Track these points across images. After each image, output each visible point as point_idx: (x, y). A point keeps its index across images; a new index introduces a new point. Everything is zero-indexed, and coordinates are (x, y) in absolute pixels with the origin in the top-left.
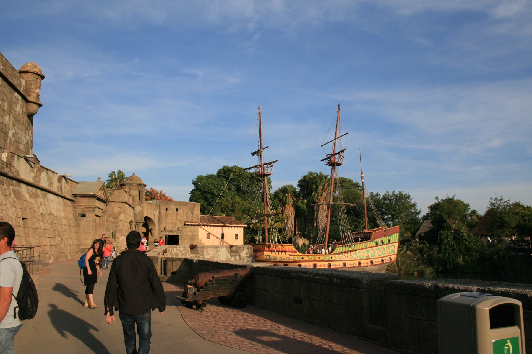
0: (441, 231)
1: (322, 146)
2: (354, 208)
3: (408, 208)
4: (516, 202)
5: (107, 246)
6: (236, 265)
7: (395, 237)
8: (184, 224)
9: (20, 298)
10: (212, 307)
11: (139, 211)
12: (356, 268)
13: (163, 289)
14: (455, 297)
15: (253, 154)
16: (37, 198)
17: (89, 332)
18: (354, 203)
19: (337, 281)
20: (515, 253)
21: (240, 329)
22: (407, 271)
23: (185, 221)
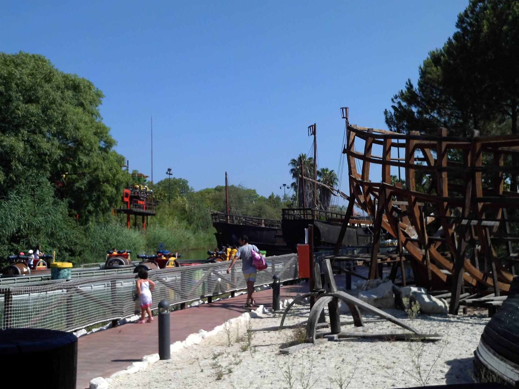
0: (476, 382)
2: (117, 323)
3: (446, 327)
5: (272, 307)
7: (371, 163)
8: (182, 309)
10: (358, 333)
11: (282, 217)
13: (148, 354)
16: (284, 342)
20: (401, 258)
23: (216, 353)
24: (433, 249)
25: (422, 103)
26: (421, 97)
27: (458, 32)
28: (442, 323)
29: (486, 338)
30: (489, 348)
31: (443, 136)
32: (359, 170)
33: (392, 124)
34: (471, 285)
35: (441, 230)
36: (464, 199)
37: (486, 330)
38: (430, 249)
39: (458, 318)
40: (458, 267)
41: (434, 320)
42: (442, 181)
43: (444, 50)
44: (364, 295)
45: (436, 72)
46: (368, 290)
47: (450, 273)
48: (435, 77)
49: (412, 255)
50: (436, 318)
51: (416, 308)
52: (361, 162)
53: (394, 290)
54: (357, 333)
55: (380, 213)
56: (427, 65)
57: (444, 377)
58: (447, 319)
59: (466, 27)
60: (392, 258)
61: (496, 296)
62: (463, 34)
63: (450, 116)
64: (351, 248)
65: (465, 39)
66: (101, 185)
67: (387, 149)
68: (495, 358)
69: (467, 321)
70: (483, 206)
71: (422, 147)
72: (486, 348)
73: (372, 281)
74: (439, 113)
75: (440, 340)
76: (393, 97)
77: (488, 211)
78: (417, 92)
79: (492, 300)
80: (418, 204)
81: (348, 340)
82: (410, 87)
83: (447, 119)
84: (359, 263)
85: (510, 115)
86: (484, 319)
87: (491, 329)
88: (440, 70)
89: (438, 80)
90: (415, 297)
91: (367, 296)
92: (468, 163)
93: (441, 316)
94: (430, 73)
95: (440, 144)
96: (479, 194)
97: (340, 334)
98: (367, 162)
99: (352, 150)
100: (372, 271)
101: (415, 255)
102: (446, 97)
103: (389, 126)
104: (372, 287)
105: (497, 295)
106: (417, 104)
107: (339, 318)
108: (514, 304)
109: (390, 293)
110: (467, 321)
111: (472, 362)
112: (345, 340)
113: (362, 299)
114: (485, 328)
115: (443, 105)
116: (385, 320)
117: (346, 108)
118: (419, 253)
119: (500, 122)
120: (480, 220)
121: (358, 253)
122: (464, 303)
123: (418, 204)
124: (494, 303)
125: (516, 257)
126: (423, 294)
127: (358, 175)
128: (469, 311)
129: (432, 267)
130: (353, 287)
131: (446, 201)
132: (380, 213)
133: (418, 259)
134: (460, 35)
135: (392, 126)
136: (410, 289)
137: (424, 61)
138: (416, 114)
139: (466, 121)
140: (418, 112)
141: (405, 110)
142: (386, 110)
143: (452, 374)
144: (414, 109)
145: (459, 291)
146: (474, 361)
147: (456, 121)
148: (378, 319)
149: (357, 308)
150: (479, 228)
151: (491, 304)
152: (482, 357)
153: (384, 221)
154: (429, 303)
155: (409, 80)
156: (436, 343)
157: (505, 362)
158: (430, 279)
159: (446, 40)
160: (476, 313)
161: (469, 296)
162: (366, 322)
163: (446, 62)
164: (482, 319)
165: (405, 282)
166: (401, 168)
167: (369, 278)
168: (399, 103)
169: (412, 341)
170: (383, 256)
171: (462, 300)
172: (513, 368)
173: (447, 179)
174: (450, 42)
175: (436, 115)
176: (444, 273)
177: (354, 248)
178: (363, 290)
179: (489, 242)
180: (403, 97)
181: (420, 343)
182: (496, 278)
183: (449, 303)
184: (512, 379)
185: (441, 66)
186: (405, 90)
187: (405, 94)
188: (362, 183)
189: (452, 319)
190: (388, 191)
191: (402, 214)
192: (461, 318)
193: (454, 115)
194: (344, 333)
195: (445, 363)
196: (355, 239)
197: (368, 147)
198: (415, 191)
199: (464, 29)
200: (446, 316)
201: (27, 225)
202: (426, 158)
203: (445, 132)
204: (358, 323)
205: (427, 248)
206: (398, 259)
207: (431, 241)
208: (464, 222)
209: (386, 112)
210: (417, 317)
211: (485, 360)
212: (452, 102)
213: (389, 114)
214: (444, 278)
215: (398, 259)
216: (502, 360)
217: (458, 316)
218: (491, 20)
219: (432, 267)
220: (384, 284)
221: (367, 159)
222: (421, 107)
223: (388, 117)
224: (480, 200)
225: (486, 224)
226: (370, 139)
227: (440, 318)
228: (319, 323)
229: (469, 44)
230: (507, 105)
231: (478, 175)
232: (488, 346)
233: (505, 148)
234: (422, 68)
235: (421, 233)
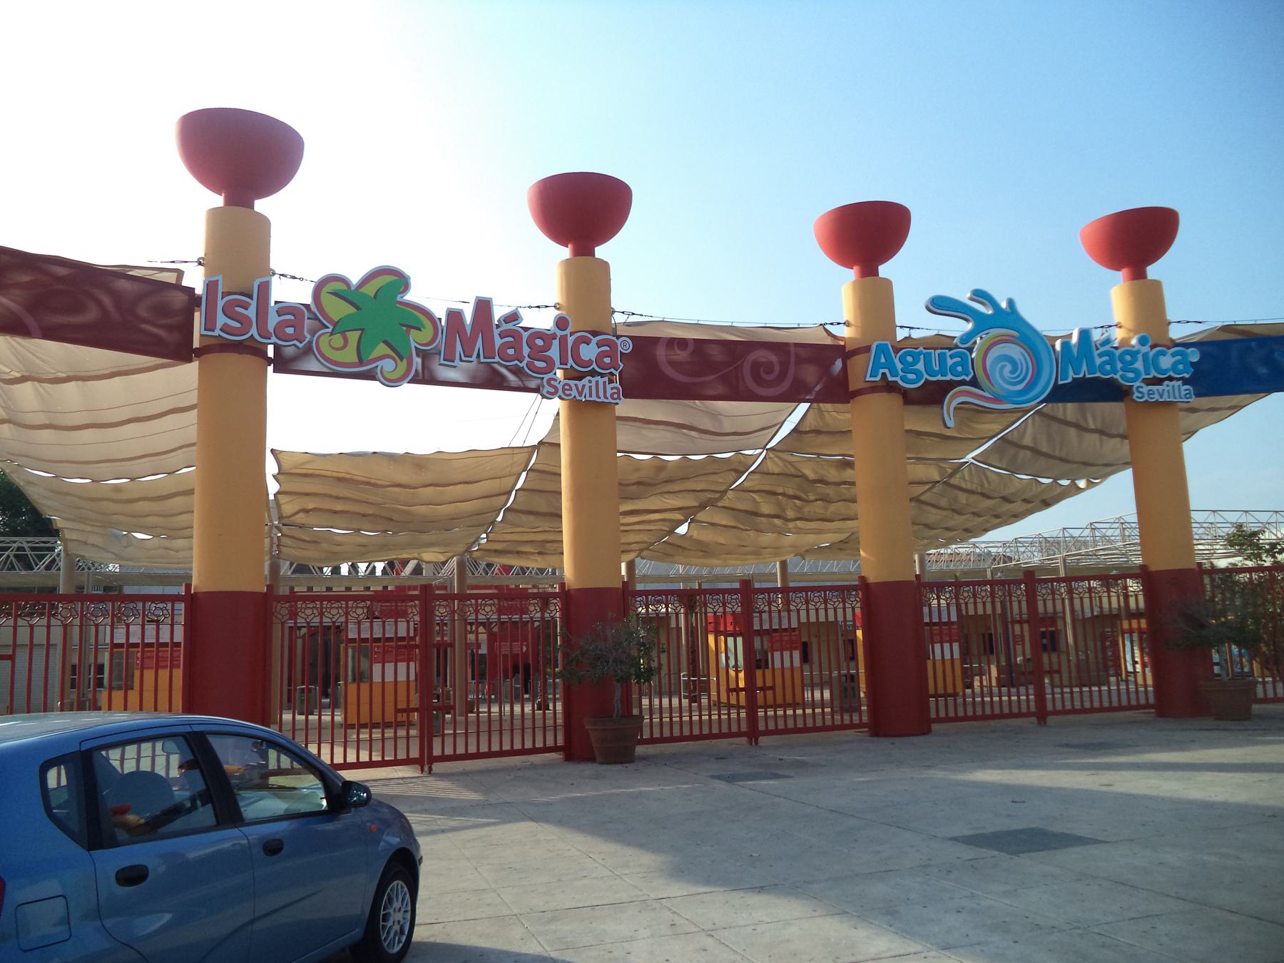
1: (1013, 802)
4: (483, 306)
7: (413, 940)
15: (911, 500)
17: (67, 783)
66: (1135, 332)
77: (955, 627)
87: (331, 944)
92: (927, 686)
114: (161, 776)
130: (1037, 417)
137: (194, 289)
166: (126, 757)
201: (1218, 678)
228: (870, 377)
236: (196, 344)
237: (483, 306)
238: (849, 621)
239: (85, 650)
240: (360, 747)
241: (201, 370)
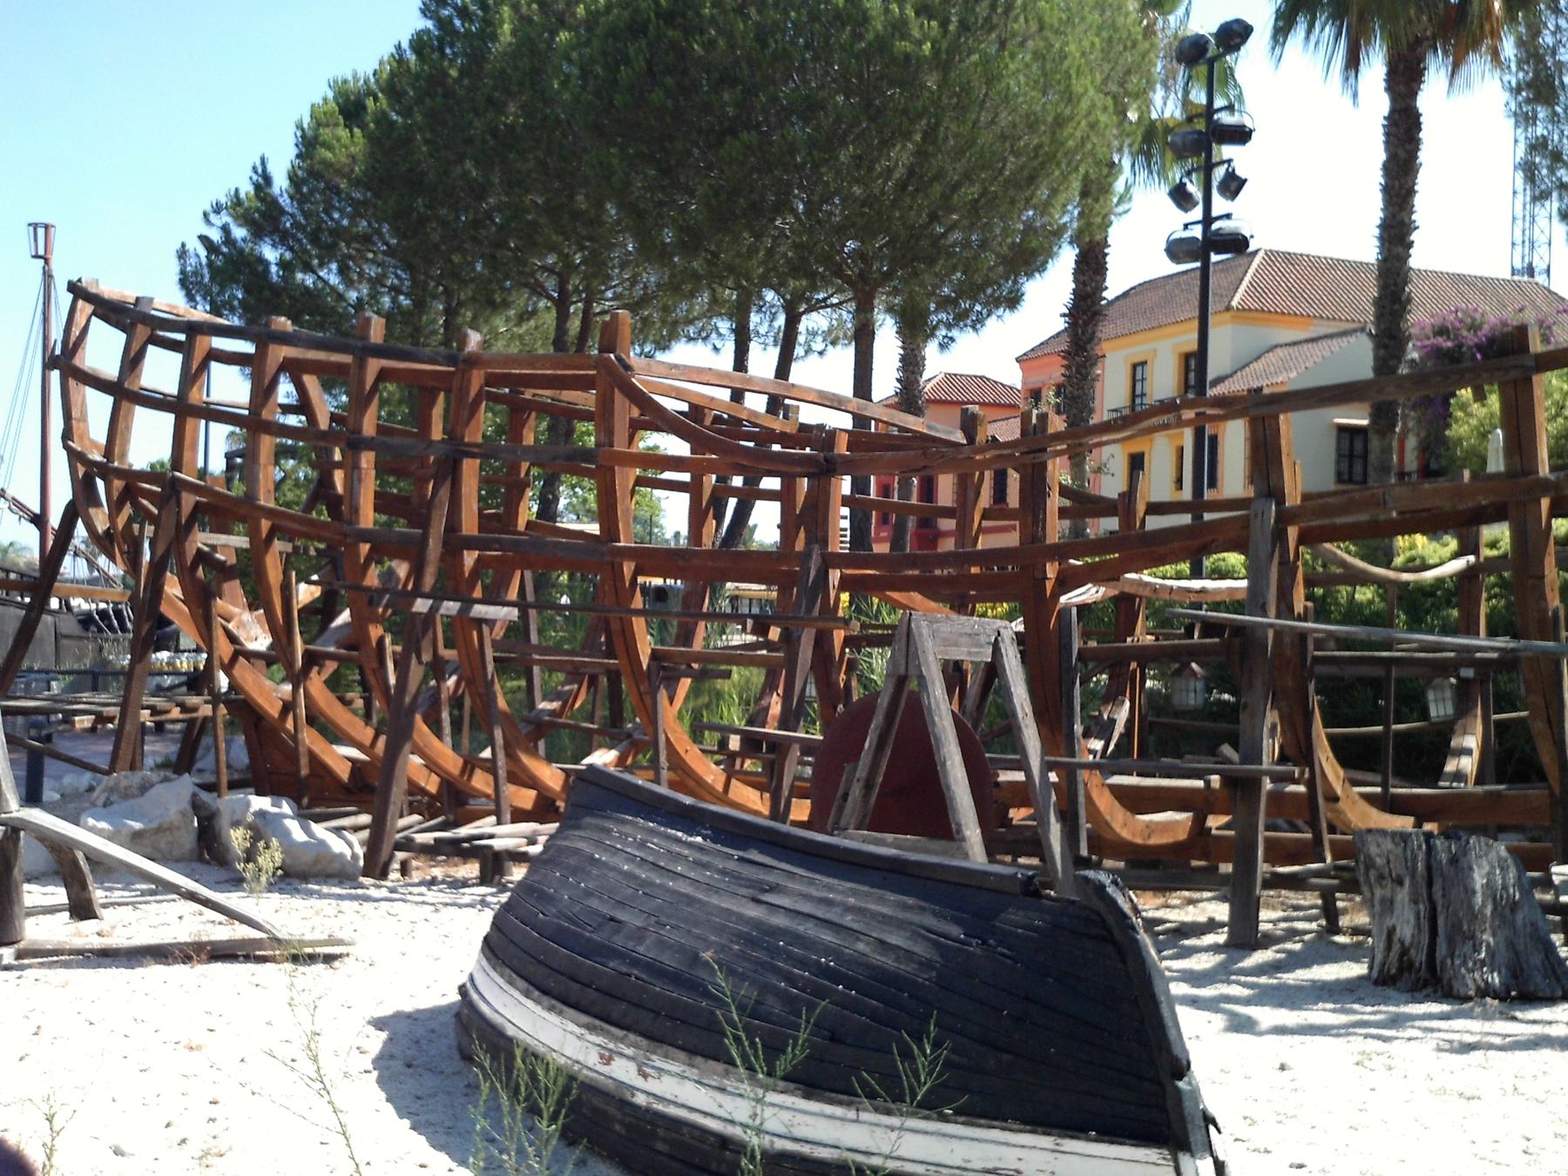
4: (1064, 315)
6: (1411, 192)
9: (1323, 29)
12: (714, 1084)
14: (1196, 765)
18: (819, 1004)
19: (821, 211)
20: (215, 710)
21: (1185, 1063)
22: (1133, 62)
24: (316, 683)
25: (294, 237)
26: (293, 216)
27: (427, 31)
28: (346, 904)
29: (497, 948)
30: (510, 976)
31: (373, 340)
32: (97, 428)
33: (197, 291)
34: (423, 792)
35: (346, 625)
36: (424, 539)
37: (497, 924)
38: (308, 683)
39: (392, 890)
40: (397, 733)
41: (322, 896)
42: (360, 480)
43: (377, 81)
44: (98, 820)
45: (349, 144)
46: (112, 803)
47: (363, 757)
48: (343, 159)
49: (253, 699)
50: (325, 889)
51: (268, 860)
52: (109, 400)
53: (196, 806)
54: (79, 943)
55: (158, 569)
56: (320, 119)
57: (370, 1067)
58: (360, 891)
59: (450, 17)
60: (184, 708)
61: (499, 823)
62: (440, 39)
63: (376, 282)
64: (43, 676)
65: (443, 55)
67: (195, 367)
68: (530, 1003)
69: (420, 899)
70: (479, 560)
71: (294, 369)
72: (502, 976)
73: (126, 777)
74: (343, 271)
75: (348, 955)
76: (209, 209)
78: (285, 201)
79: (491, 836)
80: (279, 546)
81: (51, 965)
82: (263, 181)
83: (365, 291)
84: (82, 721)
85: (550, 298)
86: (466, 890)
88: (362, 140)
89: (352, 171)
90: (261, 829)
91: (111, 823)
93: (340, 884)
94: (329, 148)
95: (361, 365)
96: (469, 525)
97: (22, 945)
98: (125, 404)
99: (77, 362)
100: (123, 745)
101: (260, 701)
102: (370, 224)
103: (190, 298)
104: (126, 795)
105: (503, 820)
106: (282, 238)
107: (19, 893)
108: (582, 845)
109: (183, 813)
110: (420, 899)
111: (449, 1019)
112: (42, 965)
113: (92, 830)
115: (357, 250)
116: (175, 896)
117: (47, 227)
118: (270, 692)
119: (523, 317)
120: (469, 602)
121: (64, 691)
122: (407, 844)
123: (279, 546)
124: (497, 844)
125: (554, 711)
126: (285, 816)
127: (95, 444)
128: (417, 869)
129: (310, 739)
130: (49, 794)
131: (366, 541)
132: (158, 569)
133: (266, 712)
134: (430, 39)
135: (198, 298)
136: (248, 804)
138: (274, 269)
139: (420, 305)
140: (282, 264)
141: (241, 251)
142: (183, 245)
143: (392, 1057)
144: (270, 253)
145: (393, 809)
146: (458, 1015)
147: (394, 301)
148: (143, 893)
149: (82, 862)
150: (463, 626)
151: (490, 847)
152: (488, 1003)
153: (167, 595)
154: (305, 844)
155: (263, 162)
156: (336, 964)
157: (560, 1013)
158: (304, 772)
159: (387, 50)
160: (438, 872)
161: (420, 823)
162: (104, 906)
163: (381, 118)
164: (462, 891)
165: (224, 780)
167: (112, 769)
168: (225, 229)
169: (264, 960)
170: (157, 701)
171: (401, 835)
172: (583, 1031)
173: (373, 472)
174: (399, 59)
175: (334, 279)
176: (341, 757)
177: (52, 675)
178: (94, 805)
179: (490, 667)
180: (240, 210)
181: (289, 966)
182: (502, 773)
183: (362, 843)
184: (578, 1062)
185: (363, 127)
186: (246, 189)
187: (246, 204)
188: (106, 471)
189: (373, 892)
190: (188, 501)
191: (225, 572)
192: (400, 890)
193: (389, 283)
194: (35, 942)
195: (369, 1023)
196: (50, 648)
197: (132, 354)
198: (272, 505)
199: (443, 24)
200: (354, 884)
202: (303, 406)
203: (377, 331)
204: (82, 909)
205: (298, 678)
206: (207, 710)
207: (312, 659)
208: (421, 605)
209: (182, 254)
210: (271, 888)
211: (497, 1011)
212: (386, 244)
213: (193, 261)
214: (343, 772)
215: (207, 710)
216: (551, 1009)
217: (388, 884)
218: (524, 10)
219: (310, 739)
220: (166, 785)
221: (124, 392)
222: (291, 249)
223: (189, 269)
224: (470, 543)
225: (482, 616)
226: (142, 332)
227: (343, 892)
229: (454, 73)
230: (544, 268)
231: (470, 470)
232: (508, 971)
233: (546, 394)
234: (306, 126)
235: (281, 635)
236: (594, 528)
237: (1064, 315)
238: (769, 495)
239: (1007, 1144)
240: (1371, 290)
241: (1356, 267)
